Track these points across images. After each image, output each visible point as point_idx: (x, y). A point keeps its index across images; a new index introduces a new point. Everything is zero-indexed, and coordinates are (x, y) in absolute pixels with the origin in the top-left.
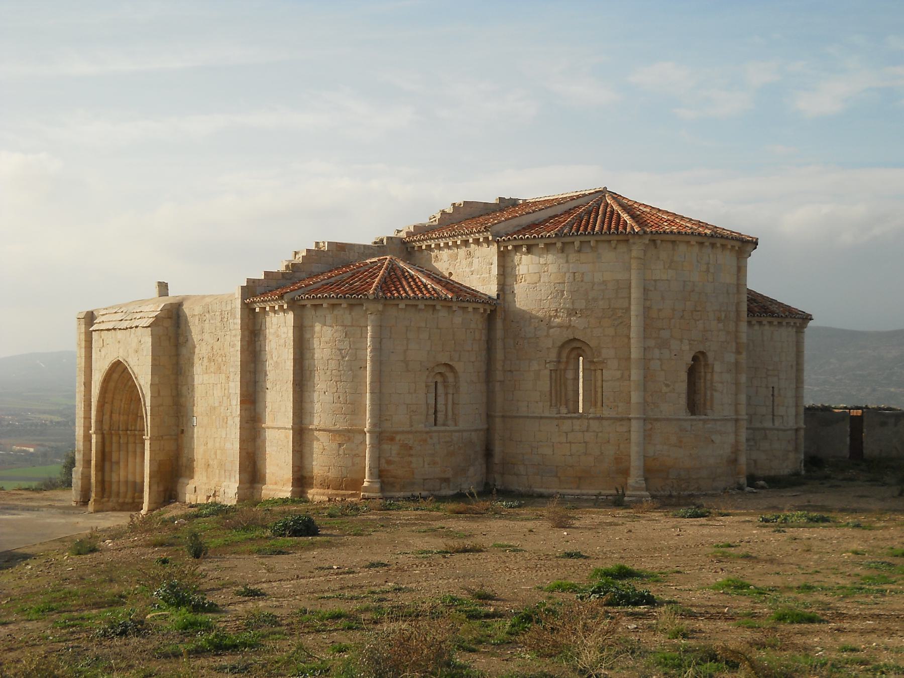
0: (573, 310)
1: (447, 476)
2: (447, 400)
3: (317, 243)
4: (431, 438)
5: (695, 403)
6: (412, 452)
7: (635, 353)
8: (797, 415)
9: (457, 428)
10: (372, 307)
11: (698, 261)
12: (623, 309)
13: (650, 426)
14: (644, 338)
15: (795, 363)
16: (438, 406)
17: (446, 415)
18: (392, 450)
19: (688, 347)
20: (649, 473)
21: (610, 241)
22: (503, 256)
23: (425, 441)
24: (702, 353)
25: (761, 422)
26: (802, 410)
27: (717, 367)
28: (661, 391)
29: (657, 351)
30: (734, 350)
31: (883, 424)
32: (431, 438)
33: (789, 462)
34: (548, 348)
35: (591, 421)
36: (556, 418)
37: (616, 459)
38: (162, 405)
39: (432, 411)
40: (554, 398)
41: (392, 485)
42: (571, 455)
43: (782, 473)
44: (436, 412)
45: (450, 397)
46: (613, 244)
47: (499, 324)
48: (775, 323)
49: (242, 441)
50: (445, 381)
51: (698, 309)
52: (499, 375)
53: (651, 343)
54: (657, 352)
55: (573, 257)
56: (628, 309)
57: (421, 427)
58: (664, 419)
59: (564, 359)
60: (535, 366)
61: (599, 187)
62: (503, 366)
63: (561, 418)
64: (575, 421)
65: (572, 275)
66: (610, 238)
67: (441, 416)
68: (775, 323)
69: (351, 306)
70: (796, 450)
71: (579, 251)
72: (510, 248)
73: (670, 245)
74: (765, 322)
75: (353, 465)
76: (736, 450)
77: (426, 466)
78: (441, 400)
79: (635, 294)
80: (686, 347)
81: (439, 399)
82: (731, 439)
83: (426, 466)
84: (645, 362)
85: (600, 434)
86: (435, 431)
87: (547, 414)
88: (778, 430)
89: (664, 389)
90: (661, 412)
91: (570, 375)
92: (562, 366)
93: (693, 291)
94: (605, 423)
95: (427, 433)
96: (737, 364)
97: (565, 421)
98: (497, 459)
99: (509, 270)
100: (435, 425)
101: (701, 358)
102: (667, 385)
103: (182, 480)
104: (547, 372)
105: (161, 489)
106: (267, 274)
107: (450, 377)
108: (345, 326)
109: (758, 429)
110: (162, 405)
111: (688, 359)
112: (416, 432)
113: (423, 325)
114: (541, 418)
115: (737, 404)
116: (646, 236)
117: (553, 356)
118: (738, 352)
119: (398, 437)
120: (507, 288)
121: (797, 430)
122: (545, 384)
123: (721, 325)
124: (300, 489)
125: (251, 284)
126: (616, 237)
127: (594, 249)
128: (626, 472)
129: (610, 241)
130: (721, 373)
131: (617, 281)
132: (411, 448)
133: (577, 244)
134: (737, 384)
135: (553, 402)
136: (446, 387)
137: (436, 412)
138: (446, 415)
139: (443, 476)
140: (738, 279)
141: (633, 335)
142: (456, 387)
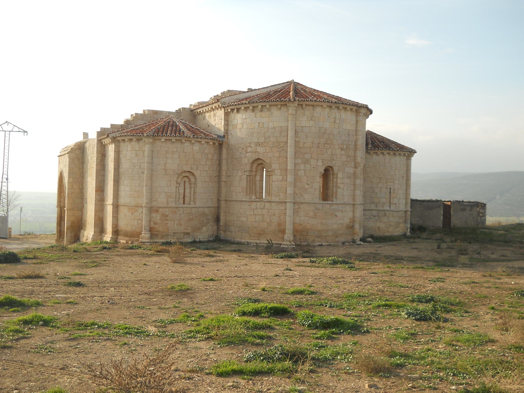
0: (258, 143)
1: (188, 231)
2: (191, 191)
3: (144, 111)
4: (179, 211)
5: (326, 194)
6: (168, 218)
7: (290, 166)
8: (406, 203)
9: (195, 206)
10: (147, 140)
11: (328, 117)
12: (283, 142)
13: (298, 207)
14: (295, 158)
15: (405, 175)
17: (190, 199)
18: (157, 217)
19: (321, 164)
20: (296, 232)
21: (277, 105)
22: (227, 114)
23: (175, 212)
24: (331, 167)
25: (383, 207)
26: (409, 201)
27: (340, 175)
30: (353, 166)
31: (463, 210)
32: (179, 211)
33: (401, 228)
34: (246, 164)
35: (266, 203)
36: (249, 202)
37: (278, 224)
38: (74, 193)
39: (182, 196)
40: (248, 190)
41: (157, 236)
42: (255, 222)
43: (395, 234)
44: (184, 198)
45: (192, 189)
46: (279, 106)
47: (224, 151)
48: (392, 154)
49: (96, 211)
50: (190, 180)
51: (328, 142)
52: (224, 178)
53: (299, 161)
54: (302, 166)
55: (259, 114)
56: (287, 142)
57: (173, 205)
58: (306, 203)
59: (254, 170)
60: (240, 174)
61: (289, 79)
62: (227, 173)
63: (251, 201)
64: (258, 203)
65: (258, 124)
66: (276, 103)
67: (187, 199)
68: (392, 154)
69: (138, 140)
70: (405, 222)
71: (261, 111)
72: (229, 110)
73: (311, 108)
74: (385, 153)
75: (138, 224)
76: (353, 221)
77: (175, 225)
78: (187, 191)
79: (291, 133)
80: (320, 164)
81: (186, 190)
82: (350, 214)
83: (175, 225)
84: (296, 170)
85: (270, 211)
86: (181, 207)
87: (244, 199)
88: (392, 211)
89: (306, 186)
90: (304, 199)
91: (258, 178)
92: (254, 174)
93: (325, 133)
94: (273, 204)
95: (176, 208)
96: (355, 173)
97: (253, 203)
98: (222, 223)
99: (230, 122)
100: (184, 204)
101: (331, 170)
102: (308, 184)
103: (82, 231)
104: (245, 176)
105: (73, 235)
106: (112, 125)
107: (193, 180)
108: (136, 151)
109: (381, 210)
110: (74, 193)
111: (322, 170)
112: (170, 207)
113: (175, 150)
114: (242, 201)
115: (354, 196)
116: (295, 102)
117: (248, 168)
118: (356, 167)
119: (160, 210)
120: (229, 132)
121: (406, 212)
122: (244, 183)
123: (343, 152)
124: (116, 236)
125: (103, 130)
126: (279, 103)
127: (269, 110)
128: (283, 232)
129: (277, 105)
130: (343, 178)
131: (281, 127)
132: (167, 216)
133: (260, 107)
134: (354, 185)
135: (248, 193)
136: (190, 184)
137: (184, 198)
138: (190, 199)
139: (185, 231)
140: (356, 127)
141: (288, 156)
142: (195, 183)
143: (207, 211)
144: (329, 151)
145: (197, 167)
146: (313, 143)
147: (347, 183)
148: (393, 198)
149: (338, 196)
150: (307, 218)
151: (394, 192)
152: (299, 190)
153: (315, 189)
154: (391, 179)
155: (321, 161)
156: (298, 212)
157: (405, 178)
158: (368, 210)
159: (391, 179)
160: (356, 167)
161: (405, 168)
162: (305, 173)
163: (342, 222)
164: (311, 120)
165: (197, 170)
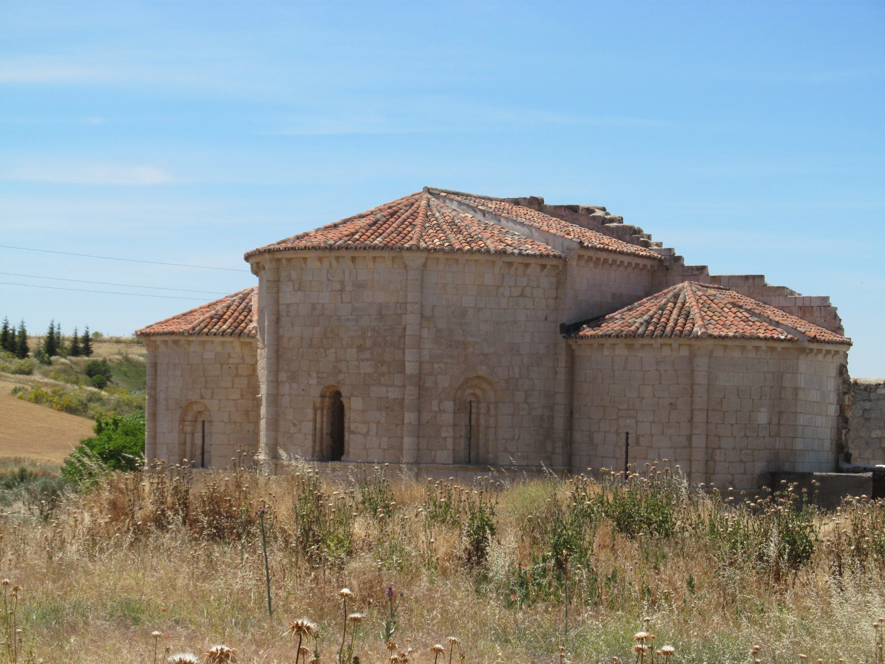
81: (206, 438)
89: (293, 430)
102: (295, 425)
123: (367, 355)
130: (363, 411)
145: (213, 394)
151: (637, 443)
153: (305, 435)
159: (627, 409)
165: (212, 398)
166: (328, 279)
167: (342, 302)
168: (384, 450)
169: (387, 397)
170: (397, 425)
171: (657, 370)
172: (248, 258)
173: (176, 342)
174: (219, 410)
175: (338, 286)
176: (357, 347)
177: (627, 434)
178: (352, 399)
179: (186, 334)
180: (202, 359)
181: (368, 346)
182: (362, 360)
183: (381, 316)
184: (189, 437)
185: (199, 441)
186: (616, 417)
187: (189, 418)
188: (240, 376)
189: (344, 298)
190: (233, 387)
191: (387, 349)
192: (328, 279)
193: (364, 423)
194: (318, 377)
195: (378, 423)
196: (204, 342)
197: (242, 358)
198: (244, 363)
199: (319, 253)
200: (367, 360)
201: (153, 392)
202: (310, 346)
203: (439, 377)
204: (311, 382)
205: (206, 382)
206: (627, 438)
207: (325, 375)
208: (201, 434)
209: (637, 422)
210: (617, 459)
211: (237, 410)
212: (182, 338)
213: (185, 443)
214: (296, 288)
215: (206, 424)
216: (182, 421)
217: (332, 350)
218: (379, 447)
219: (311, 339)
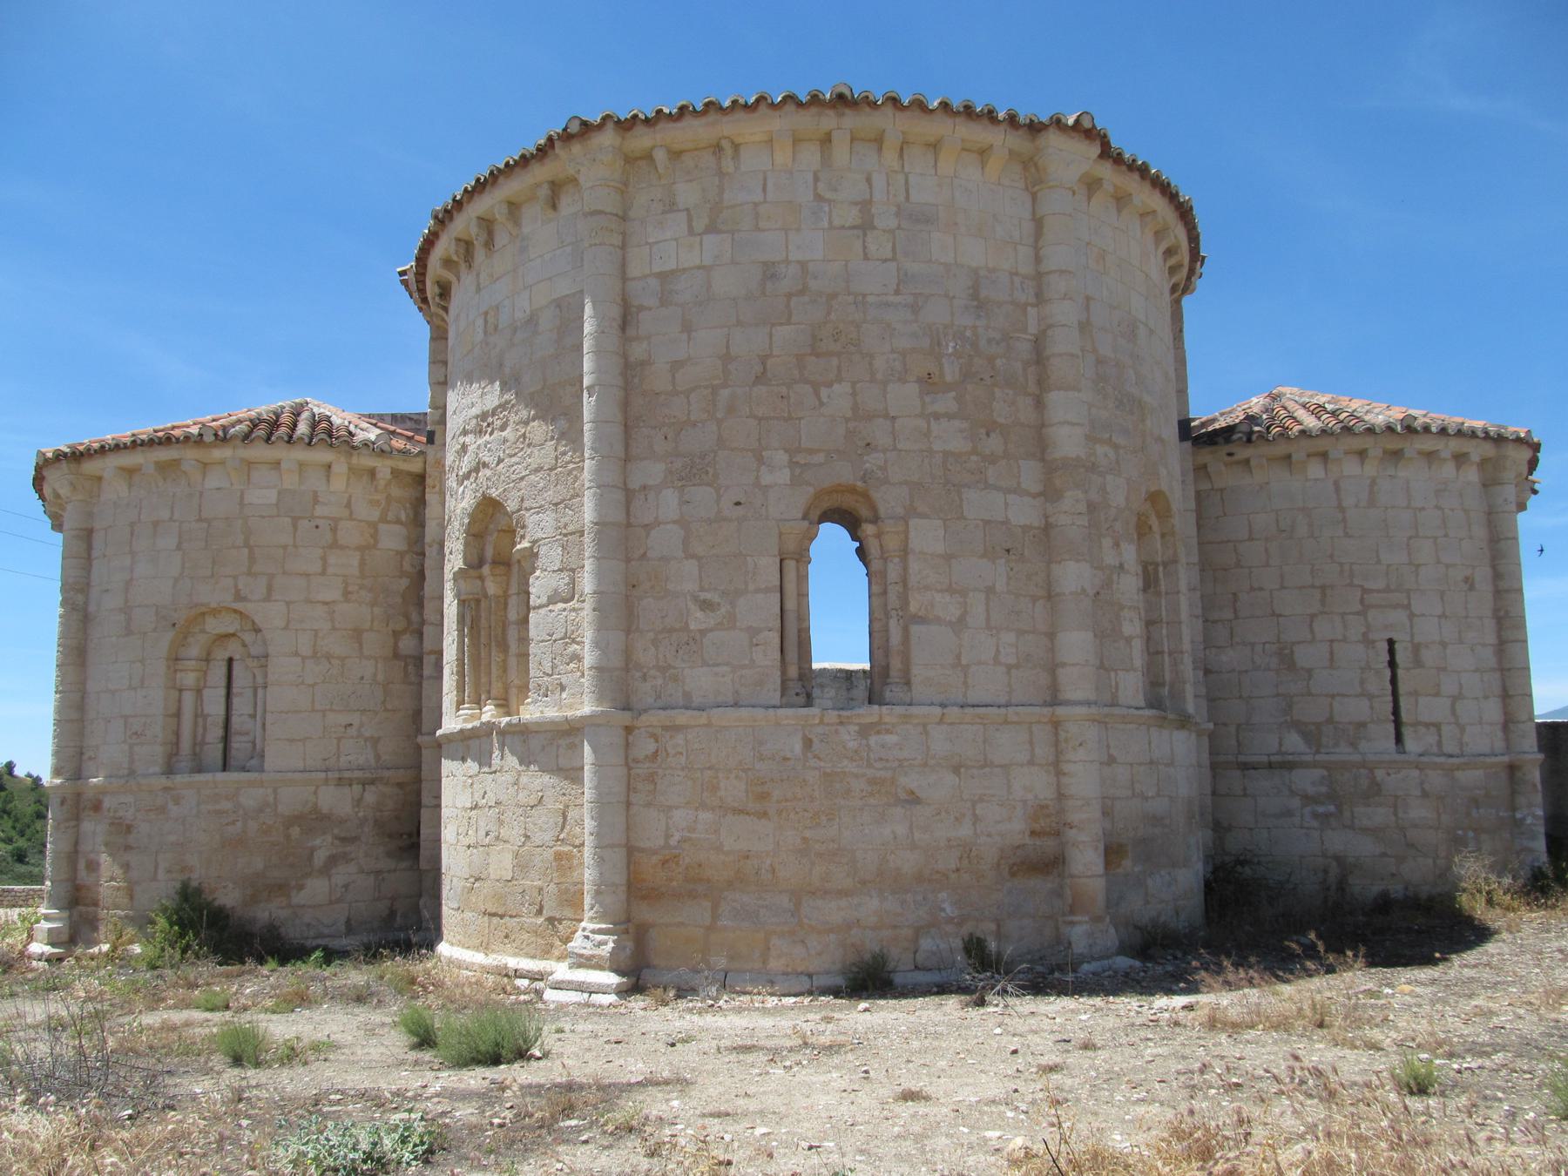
16: (235, 720)
19: (784, 476)
23: (162, 810)
25: (1353, 745)
28: (686, 628)
29: (670, 498)
54: (669, 502)
81: (236, 701)
89: (698, 620)
102: (706, 606)
113: (165, 514)
118: (1050, 494)
123: (946, 403)
130: (948, 557)
143: (334, 800)
144: (838, 398)
145: (270, 588)
146: (727, 358)
147: (990, 591)
148: (1415, 694)
149: (915, 670)
150: (705, 816)
151: (1418, 663)
152: (655, 643)
153: (753, 632)
154: (1388, 590)
155: (781, 457)
156: (651, 778)
157: (1485, 587)
158: (1270, 766)
159: (1388, 590)
160: (1050, 494)
161: (1480, 532)
162: (686, 542)
163: (965, 831)
164: (712, 229)
165: (268, 598)
166: (819, 198)
167: (866, 257)
168: (1009, 667)
169: (1006, 522)
170: (1034, 599)
171: (1437, 507)
172: (64, 476)
173: (164, 468)
174: (286, 628)
175: (852, 216)
176: (919, 381)
177: (1391, 643)
178: (913, 522)
179: (209, 438)
180: (242, 504)
181: (948, 378)
182: (937, 416)
183: (979, 303)
184: (188, 699)
185: (215, 707)
186: (1358, 607)
187: (194, 651)
188: (342, 548)
189: (872, 248)
190: (323, 573)
191: (998, 392)
192: (819, 198)
193: (950, 590)
194: (792, 464)
195: (990, 591)
196: (250, 464)
197: (348, 505)
198: (351, 518)
199: (806, 121)
200: (950, 417)
201: (80, 598)
202: (760, 379)
203: (1109, 478)
204: (767, 479)
205: (252, 559)
206: (1392, 652)
207: (820, 458)
208: (223, 692)
209: (1412, 616)
210: (1371, 697)
211: (334, 628)
212: (190, 454)
213: (178, 715)
214: (699, 226)
215: (237, 667)
216: (175, 659)
217: (845, 388)
218: (996, 662)
219: (763, 360)
